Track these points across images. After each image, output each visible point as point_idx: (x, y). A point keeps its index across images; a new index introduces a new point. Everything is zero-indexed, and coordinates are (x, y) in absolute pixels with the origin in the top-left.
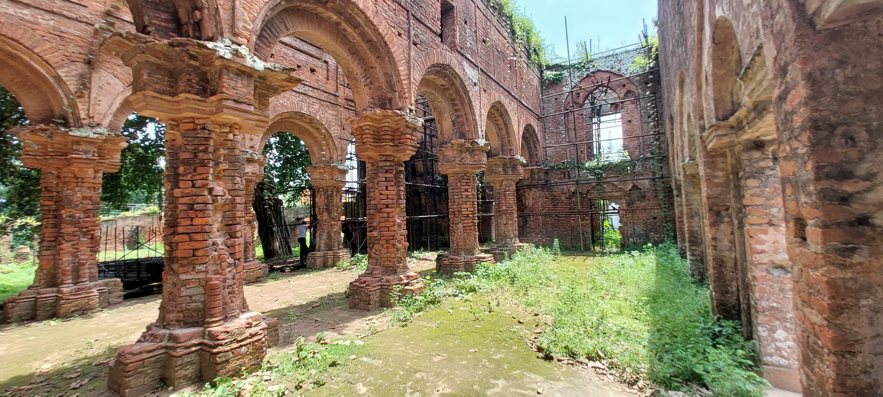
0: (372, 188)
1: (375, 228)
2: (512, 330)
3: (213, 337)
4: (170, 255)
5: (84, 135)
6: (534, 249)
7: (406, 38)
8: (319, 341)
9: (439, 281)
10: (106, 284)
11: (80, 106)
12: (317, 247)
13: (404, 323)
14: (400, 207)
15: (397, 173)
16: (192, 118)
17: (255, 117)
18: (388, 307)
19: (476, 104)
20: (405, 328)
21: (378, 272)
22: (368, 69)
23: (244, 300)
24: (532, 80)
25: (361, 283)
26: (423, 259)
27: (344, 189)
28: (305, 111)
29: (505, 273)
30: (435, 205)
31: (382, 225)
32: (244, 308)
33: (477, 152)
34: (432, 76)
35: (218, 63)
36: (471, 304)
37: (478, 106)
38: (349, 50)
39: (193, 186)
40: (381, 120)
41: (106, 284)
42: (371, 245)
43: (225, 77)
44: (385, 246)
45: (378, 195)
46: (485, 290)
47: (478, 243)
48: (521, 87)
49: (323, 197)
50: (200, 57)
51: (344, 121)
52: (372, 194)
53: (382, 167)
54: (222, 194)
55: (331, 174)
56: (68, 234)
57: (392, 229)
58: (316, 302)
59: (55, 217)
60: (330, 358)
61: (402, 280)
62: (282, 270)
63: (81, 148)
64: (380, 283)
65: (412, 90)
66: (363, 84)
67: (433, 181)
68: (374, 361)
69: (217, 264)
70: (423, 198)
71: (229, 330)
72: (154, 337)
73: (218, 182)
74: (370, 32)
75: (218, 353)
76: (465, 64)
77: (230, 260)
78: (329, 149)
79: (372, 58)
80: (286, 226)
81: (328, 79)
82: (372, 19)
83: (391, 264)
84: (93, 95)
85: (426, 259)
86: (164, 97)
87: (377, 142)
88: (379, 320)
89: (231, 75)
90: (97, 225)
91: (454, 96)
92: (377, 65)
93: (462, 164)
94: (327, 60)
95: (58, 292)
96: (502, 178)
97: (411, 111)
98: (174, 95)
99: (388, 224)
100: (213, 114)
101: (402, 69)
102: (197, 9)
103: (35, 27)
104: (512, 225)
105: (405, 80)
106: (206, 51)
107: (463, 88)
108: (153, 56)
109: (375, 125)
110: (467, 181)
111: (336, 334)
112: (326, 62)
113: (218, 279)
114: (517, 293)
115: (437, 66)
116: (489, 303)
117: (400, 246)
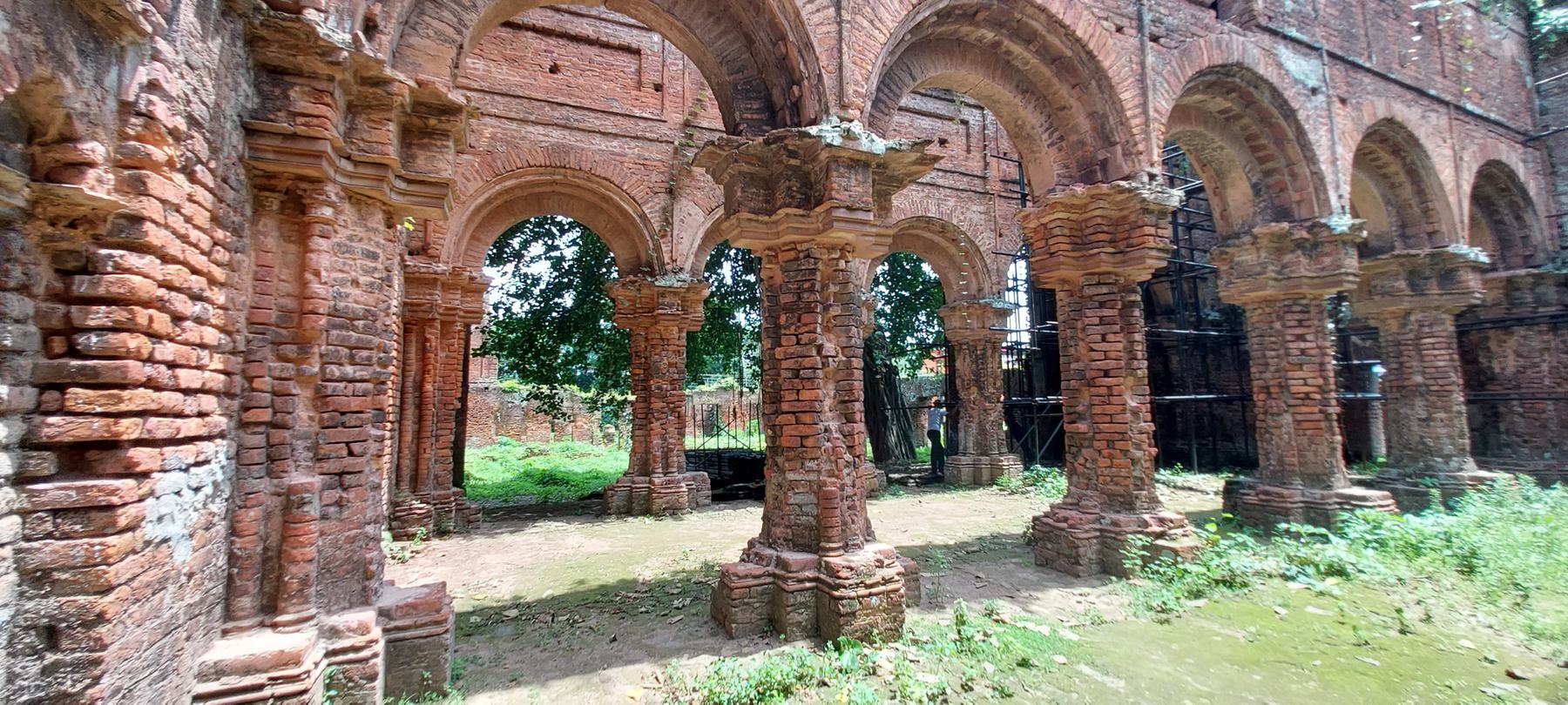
0: (1072, 338)
1: (1080, 417)
2: (1490, 691)
3: (832, 571)
4: (773, 442)
5: (668, 284)
6: (1535, 491)
7: (1133, 32)
8: (990, 615)
9: (1241, 538)
10: (694, 479)
11: (664, 249)
12: (961, 448)
13: (1164, 616)
14: (1135, 376)
15: (1124, 307)
16: (794, 243)
17: (874, 230)
18: (1120, 577)
19: (1319, 138)
20: (1166, 626)
21: (1093, 501)
22: (1054, 114)
23: (867, 521)
24: (1498, 44)
25: (1058, 521)
26: (1183, 488)
27: (1004, 344)
28: (933, 213)
29: (1438, 543)
30: (1206, 374)
31: (1097, 410)
32: (869, 535)
33: (1328, 248)
34: (1198, 97)
35: (824, 155)
36: (1341, 603)
37: (1324, 141)
38: (1017, 86)
39: (798, 343)
40: (1086, 205)
41: (694, 479)
42: (1074, 449)
43: (835, 174)
44: (1105, 452)
45: (1084, 351)
46: (1377, 578)
47: (1342, 463)
48: (1460, 71)
49: (968, 360)
50: (801, 152)
51: (1001, 221)
52: (1072, 350)
53: (1091, 297)
54: (833, 353)
55: (982, 318)
56: (658, 411)
57: (1119, 418)
58: (972, 545)
59: (645, 389)
60: (1020, 649)
61: (1146, 524)
62: (902, 483)
63: (667, 300)
64: (1097, 526)
65: (1153, 135)
66: (1046, 144)
67: (1199, 323)
68: (1106, 679)
69: (831, 462)
70: (1175, 359)
71: (853, 565)
72: (760, 558)
73: (827, 335)
74: (1057, 42)
75: (842, 598)
76: (1286, 55)
77: (848, 457)
78: (976, 274)
79: (1063, 91)
80: (904, 409)
81: (968, 151)
82: (1061, 17)
83: (1120, 490)
84: (675, 232)
85: (1190, 489)
86: (761, 218)
87: (1079, 250)
88: (1103, 598)
89: (842, 170)
90: (682, 398)
91: (1255, 129)
92: (1073, 102)
93: (1283, 275)
94: (966, 117)
95: (651, 482)
96: (1406, 305)
97: (1152, 177)
98: (771, 213)
99: (1109, 409)
100: (819, 232)
101: (1128, 96)
102: (794, 83)
103: (624, 159)
104: (1449, 423)
105: (1135, 116)
106: (808, 140)
107: (1280, 107)
108: (747, 163)
109: (1073, 217)
110: (1301, 316)
111: (1018, 609)
112: (965, 123)
113: (834, 484)
114: (1490, 597)
115: (1210, 73)
116: (1399, 611)
117: (1139, 454)
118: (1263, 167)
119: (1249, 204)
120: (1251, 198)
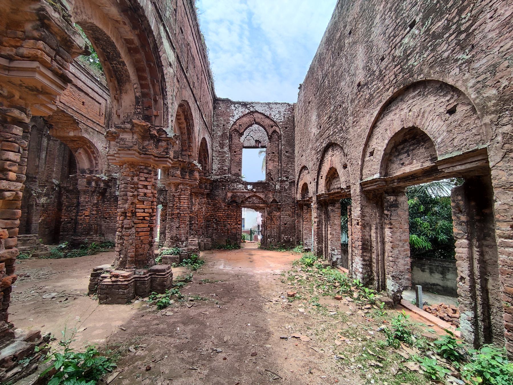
118: (143, 90)
119: (133, 107)
120: (134, 104)
